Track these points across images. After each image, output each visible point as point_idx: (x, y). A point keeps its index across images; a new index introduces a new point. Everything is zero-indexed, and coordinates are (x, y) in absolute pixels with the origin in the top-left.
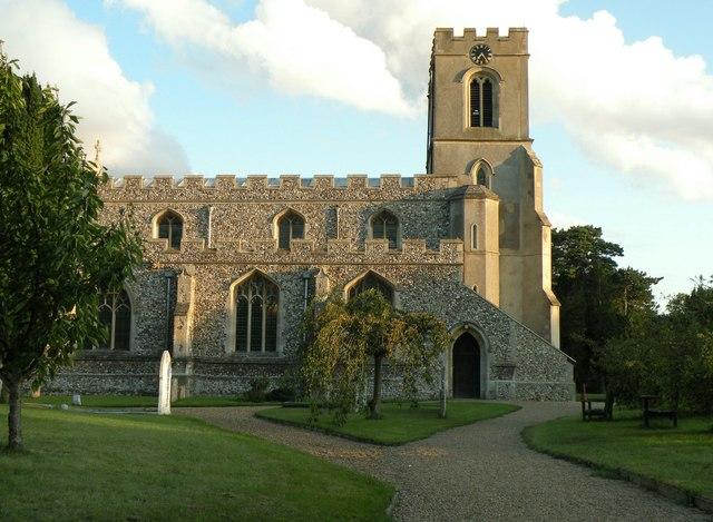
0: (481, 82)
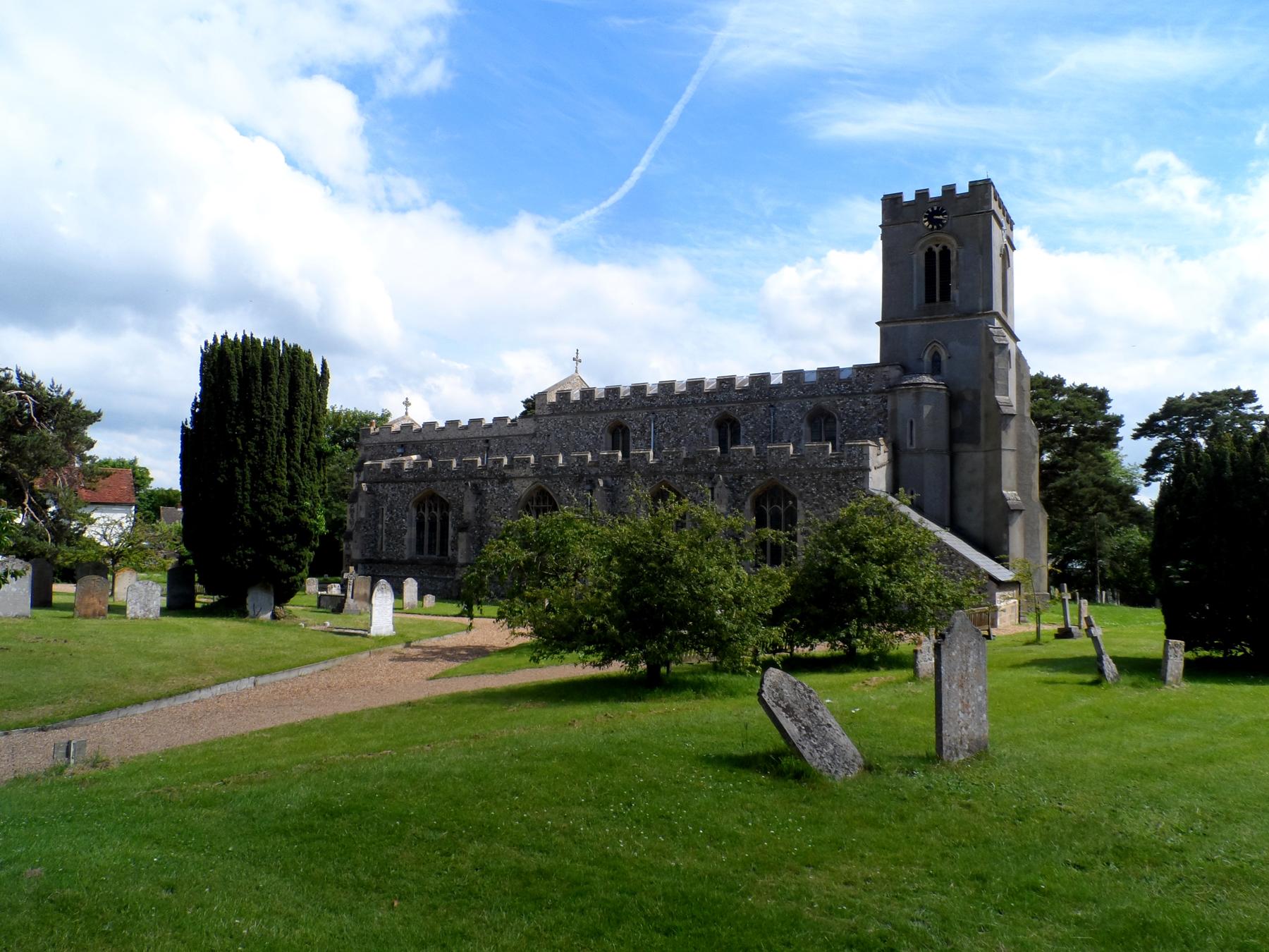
0: (937, 250)
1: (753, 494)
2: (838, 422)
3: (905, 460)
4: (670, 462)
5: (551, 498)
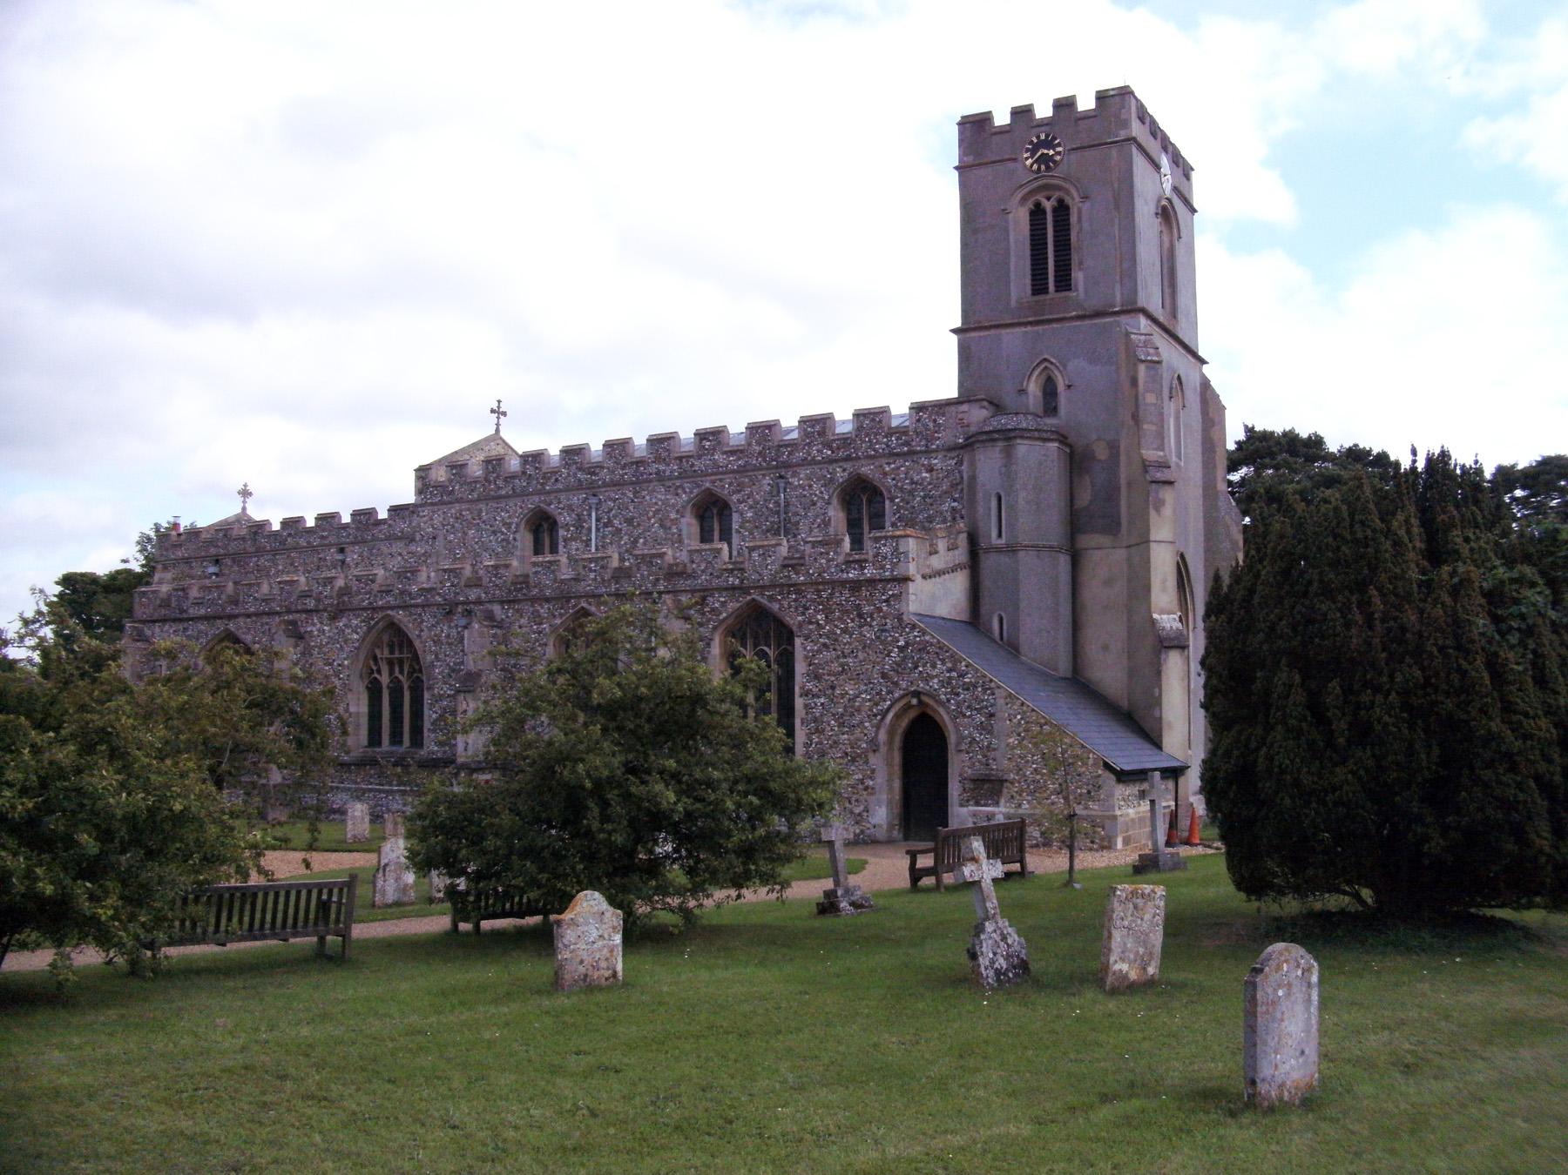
0: (1048, 206)
1: (724, 626)
2: (887, 502)
3: (988, 563)
4: (592, 575)
5: (410, 643)
